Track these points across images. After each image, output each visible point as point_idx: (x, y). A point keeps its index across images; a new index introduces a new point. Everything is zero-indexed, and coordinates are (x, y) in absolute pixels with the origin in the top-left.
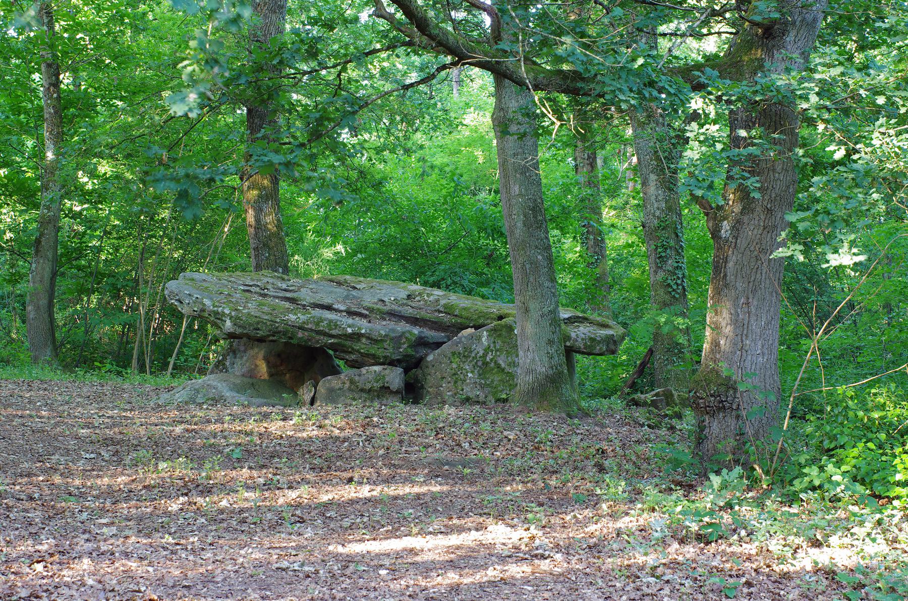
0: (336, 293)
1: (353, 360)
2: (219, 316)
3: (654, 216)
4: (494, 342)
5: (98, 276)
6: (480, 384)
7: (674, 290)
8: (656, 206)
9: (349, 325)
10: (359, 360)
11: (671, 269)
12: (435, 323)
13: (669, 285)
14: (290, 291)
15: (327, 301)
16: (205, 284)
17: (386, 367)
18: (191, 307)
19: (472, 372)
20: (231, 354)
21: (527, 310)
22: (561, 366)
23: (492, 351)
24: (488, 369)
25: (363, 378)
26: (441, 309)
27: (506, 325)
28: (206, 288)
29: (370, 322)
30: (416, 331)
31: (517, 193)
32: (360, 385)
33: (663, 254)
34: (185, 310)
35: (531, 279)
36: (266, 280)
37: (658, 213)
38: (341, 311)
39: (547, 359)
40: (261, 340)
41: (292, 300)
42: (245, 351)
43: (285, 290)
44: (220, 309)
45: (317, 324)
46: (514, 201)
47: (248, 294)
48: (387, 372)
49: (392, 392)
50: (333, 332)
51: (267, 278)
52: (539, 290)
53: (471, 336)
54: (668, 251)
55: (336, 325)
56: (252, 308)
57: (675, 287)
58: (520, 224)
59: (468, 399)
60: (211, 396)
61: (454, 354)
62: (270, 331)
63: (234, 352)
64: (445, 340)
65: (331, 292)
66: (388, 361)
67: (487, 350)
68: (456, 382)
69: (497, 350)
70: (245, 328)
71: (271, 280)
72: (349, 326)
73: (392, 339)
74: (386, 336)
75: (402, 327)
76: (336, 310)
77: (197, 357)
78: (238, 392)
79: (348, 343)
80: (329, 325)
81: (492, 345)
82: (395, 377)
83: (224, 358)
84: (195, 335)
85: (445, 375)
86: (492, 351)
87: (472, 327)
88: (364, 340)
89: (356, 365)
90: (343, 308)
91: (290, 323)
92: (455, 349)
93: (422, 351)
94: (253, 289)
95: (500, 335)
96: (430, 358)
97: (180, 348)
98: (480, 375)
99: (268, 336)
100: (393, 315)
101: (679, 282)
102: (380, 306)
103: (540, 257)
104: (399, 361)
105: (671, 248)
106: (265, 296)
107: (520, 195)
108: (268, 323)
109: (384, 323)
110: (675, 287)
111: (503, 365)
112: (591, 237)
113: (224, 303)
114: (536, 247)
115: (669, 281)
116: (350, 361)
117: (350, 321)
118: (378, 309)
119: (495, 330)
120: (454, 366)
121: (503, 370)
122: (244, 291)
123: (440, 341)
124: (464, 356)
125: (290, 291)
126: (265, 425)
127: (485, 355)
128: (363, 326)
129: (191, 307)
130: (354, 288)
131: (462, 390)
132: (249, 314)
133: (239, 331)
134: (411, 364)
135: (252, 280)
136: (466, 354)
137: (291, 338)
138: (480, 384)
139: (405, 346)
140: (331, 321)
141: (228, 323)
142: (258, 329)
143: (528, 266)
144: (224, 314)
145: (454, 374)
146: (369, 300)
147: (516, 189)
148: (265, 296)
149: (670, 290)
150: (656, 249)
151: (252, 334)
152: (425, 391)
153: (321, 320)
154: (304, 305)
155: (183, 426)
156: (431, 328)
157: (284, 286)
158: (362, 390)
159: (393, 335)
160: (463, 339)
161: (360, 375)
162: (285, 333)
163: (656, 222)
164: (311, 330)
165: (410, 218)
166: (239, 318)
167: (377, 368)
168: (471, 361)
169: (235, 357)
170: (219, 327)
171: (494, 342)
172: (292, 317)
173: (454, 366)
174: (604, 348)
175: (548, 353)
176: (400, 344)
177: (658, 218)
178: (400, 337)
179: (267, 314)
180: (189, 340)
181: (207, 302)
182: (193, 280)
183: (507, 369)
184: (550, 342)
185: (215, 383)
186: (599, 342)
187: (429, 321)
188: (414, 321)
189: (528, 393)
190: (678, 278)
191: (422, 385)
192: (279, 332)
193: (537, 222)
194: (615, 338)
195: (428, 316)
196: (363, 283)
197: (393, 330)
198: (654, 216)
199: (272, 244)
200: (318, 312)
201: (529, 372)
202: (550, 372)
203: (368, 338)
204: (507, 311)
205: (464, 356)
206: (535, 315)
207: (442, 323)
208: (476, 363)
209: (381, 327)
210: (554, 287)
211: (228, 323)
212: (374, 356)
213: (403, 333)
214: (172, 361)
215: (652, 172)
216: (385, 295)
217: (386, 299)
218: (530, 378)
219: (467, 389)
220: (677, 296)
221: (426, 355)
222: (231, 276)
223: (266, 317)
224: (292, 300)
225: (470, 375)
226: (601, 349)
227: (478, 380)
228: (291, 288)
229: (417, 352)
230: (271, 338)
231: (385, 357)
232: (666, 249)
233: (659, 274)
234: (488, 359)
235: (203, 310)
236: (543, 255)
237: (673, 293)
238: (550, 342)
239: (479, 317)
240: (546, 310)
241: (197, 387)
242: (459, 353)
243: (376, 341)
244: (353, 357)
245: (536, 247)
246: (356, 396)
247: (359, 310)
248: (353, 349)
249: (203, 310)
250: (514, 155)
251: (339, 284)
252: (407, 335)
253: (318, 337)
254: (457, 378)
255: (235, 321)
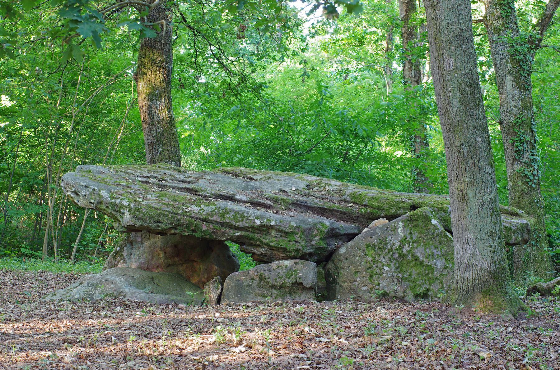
0: (234, 183)
1: (262, 254)
2: (117, 208)
3: (511, 113)
4: (411, 233)
5: (17, 177)
6: (398, 278)
7: (531, 181)
8: (512, 104)
9: (257, 217)
10: (269, 253)
11: (527, 161)
12: (344, 213)
13: (526, 176)
14: (189, 182)
15: (229, 191)
16: (102, 176)
17: (297, 261)
18: (88, 199)
19: (388, 265)
20: (128, 245)
21: (465, 198)
22: (503, 260)
23: (409, 243)
24: (405, 261)
25: (273, 273)
26: (348, 199)
27: (422, 215)
28: (103, 180)
29: (277, 213)
30: (327, 222)
31: (452, 67)
32: (271, 282)
33: (521, 148)
34: (82, 203)
35: (470, 164)
36: (163, 171)
37: (514, 111)
38: (244, 202)
39: (489, 253)
40: (162, 233)
41: (193, 191)
42: (142, 243)
43: (183, 181)
44: (118, 201)
45: (223, 216)
46: (448, 77)
47: (146, 185)
48: (299, 266)
49: (305, 289)
50: (240, 224)
51: (162, 169)
52: (478, 176)
53: (386, 228)
54: (525, 145)
55: (243, 217)
56: (152, 199)
57: (532, 178)
58: (456, 103)
59: (385, 295)
60: (109, 291)
61: (368, 246)
62: (172, 224)
63: (131, 243)
64: (356, 231)
65: (229, 183)
66: (299, 255)
67: (403, 242)
68: (371, 276)
69: (414, 242)
70: (144, 220)
71: (168, 172)
72: (257, 218)
73: (303, 231)
74: (297, 227)
75: (311, 218)
76: (240, 201)
77: (96, 242)
78: (137, 287)
79: (256, 236)
80: (235, 217)
81: (408, 236)
82: (308, 272)
83: (122, 249)
84: (94, 224)
85: (360, 269)
86: (409, 243)
87: (383, 217)
88: (273, 233)
89: (262, 260)
90: (245, 199)
91: (193, 215)
92: (369, 241)
93: (334, 244)
94: (151, 180)
95: (416, 226)
96: (343, 250)
97: (83, 234)
98: (397, 268)
99: (170, 229)
100: (298, 205)
101: (535, 173)
102: (282, 196)
103: (479, 139)
104: (311, 254)
105: (527, 142)
106: (164, 187)
107: (456, 69)
108: (170, 215)
109: (292, 214)
110: (532, 178)
111: (421, 258)
112: (418, 140)
113: (122, 194)
114: (475, 128)
115: (526, 172)
116: (258, 255)
117: (258, 213)
118: (283, 200)
119: (411, 220)
120: (369, 259)
121: (421, 263)
122: (142, 182)
123: (351, 232)
124: (379, 248)
125: (189, 182)
126: (178, 343)
127: (401, 247)
128: (272, 217)
129: (88, 199)
130: (252, 179)
131: (379, 284)
132: (149, 206)
133: (138, 224)
134: (324, 258)
135: (149, 171)
136: (381, 247)
137: (194, 231)
138: (398, 278)
139: (317, 238)
140: (237, 212)
141: (127, 216)
142: (159, 222)
143: (465, 149)
144: (122, 206)
145: (369, 268)
146: (270, 190)
147: (451, 63)
148: (164, 187)
149: (527, 180)
150: (514, 143)
151: (153, 226)
152: (338, 287)
153: (227, 211)
154: (205, 196)
155: (76, 350)
156: (340, 219)
157: (182, 177)
158: (273, 287)
159: (304, 227)
160: (378, 230)
161: (270, 270)
162: (188, 226)
163: (513, 118)
164: (216, 222)
165: (283, 121)
166: (138, 210)
167: (288, 263)
168: (387, 254)
169: (132, 248)
170: (116, 220)
171: (411, 233)
172: (195, 209)
173: (369, 259)
174: (520, 238)
175: (490, 246)
176: (312, 236)
177: (515, 115)
178: (312, 228)
179: (169, 205)
180: (89, 228)
181: (104, 193)
182: (90, 172)
183: (426, 262)
184: (492, 234)
185: (113, 278)
186: (515, 231)
187: (338, 211)
188: (321, 211)
189: (468, 291)
190: (534, 169)
191: (335, 279)
192: (182, 225)
193: (474, 100)
194: (530, 227)
195: (336, 206)
196: (260, 174)
197: (304, 222)
198: (511, 113)
199: (165, 140)
200: (221, 203)
201: (468, 267)
202: (493, 268)
203: (278, 230)
204: (419, 200)
205: (379, 248)
206: (474, 203)
207: (350, 213)
208: (392, 256)
209: (292, 219)
210: (493, 172)
211: (127, 216)
212: (284, 250)
213: (315, 224)
214: (75, 246)
215: (508, 74)
216: (285, 185)
217: (287, 189)
218: (470, 275)
219: (383, 283)
220: (534, 186)
221: (338, 247)
222: (128, 168)
223: (168, 209)
224: (193, 191)
225: (386, 268)
226: (516, 239)
227: (395, 274)
228: (189, 180)
229: (329, 245)
230: (173, 231)
231: (296, 251)
232: (523, 143)
233: (516, 166)
234: (405, 252)
235: (100, 203)
236: (481, 137)
237: (530, 183)
238: (492, 234)
239: (391, 207)
240: (486, 198)
241: (94, 282)
242: (374, 245)
243: (286, 234)
244: (262, 250)
245: (475, 128)
246: (266, 293)
247: (262, 201)
248: (261, 242)
249: (100, 203)
250: (449, 25)
251: (235, 175)
252: (319, 226)
253: (223, 230)
254: (373, 273)
255: (134, 213)
